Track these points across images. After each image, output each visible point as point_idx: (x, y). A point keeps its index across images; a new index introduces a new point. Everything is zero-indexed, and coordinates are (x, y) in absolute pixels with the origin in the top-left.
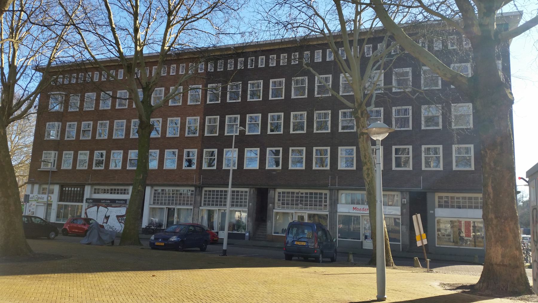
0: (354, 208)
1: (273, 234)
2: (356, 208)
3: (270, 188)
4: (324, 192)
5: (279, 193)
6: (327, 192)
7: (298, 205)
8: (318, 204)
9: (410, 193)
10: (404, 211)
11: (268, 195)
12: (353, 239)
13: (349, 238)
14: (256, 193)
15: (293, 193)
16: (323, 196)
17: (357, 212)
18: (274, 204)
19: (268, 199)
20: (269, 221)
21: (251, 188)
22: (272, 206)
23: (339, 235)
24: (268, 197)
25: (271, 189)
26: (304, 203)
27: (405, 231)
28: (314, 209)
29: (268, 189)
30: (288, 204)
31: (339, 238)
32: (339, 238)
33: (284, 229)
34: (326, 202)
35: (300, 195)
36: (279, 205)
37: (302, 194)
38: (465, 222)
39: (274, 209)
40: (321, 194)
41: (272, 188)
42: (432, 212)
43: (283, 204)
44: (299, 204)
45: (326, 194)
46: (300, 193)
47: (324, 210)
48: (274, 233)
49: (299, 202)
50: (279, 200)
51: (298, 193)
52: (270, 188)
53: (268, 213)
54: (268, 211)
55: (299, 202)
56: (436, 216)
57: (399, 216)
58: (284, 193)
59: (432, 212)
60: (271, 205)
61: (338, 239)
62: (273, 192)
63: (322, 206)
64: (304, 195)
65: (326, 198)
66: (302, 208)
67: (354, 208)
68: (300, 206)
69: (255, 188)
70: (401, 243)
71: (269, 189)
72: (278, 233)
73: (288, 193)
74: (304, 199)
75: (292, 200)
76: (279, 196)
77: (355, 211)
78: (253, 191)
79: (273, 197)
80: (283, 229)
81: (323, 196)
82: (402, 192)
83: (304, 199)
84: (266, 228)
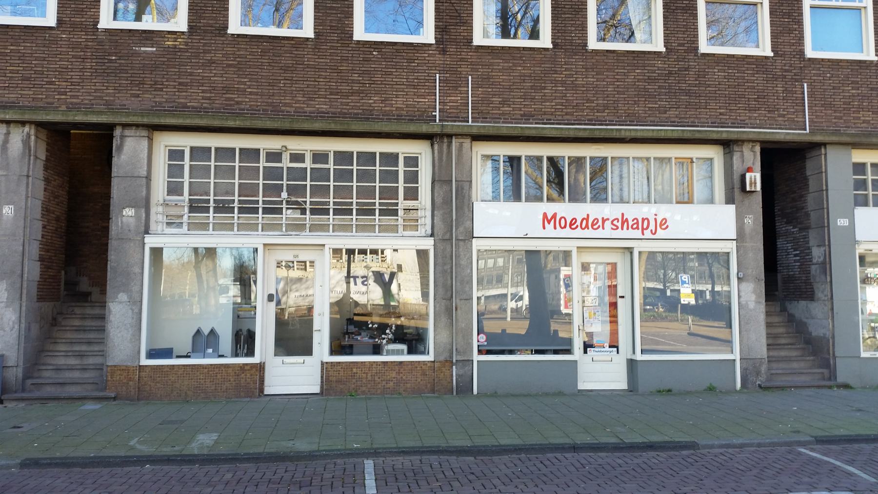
0: (545, 215)
1: (145, 362)
2: (554, 216)
3: (125, 126)
4: (403, 148)
5: (175, 154)
6: (421, 150)
7: (279, 211)
8: (354, 207)
9: (762, 142)
10: (749, 221)
11: (115, 160)
12: (538, 352)
13: (521, 352)
14: (42, 155)
15: (251, 154)
16: (401, 168)
17: (560, 233)
18: (147, 205)
19: (115, 182)
20: (123, 297)
21: (8, 122)
22: (137, 217)
23: (483, 338)
24: (114, 169)
25: (127, 132)
26: (355, 201)
27: (752, 305)
28: (241, 227)
29: (111, 127)
30: (223, 207)
31: (480, 352)
32: (480, 352)
33: (206, 331)
34: (412, 194)
35: (286, 163)
36: (173, 211)
37: (297, 157)
38: (209, 230)
39: (147, 232)
40: (391, 159)
41: (137, 126)
42: (843, 222)
43: (196, 207)
44: (284, 206)
45: (412, 161)
46: (286, 157)
47: (406, 233)
48: (151, 354)
49: (284, 195)
50: (174, 189)
51: (274, 156)
52: (125, 126)
53: (112, 256)
54: (113, 244)
55: (284, 195)
56: (858, 238)
57: (729, 244)
58: (198, 153)
59: (843, 222)
60: (129, 212)
61: (476, 357)
62: (145, 143)
63: (395, 213)
64: (308, 164)
65: (413, 177)
66: (299, 227)
67: (545, 215)
68: (289, 215)
69: (39, 125)
70: (736, 356)
71: (118, 132)
72: (167, 353)
73: (226, 153)
74: (308, 183)
75: (247, 190)
76: (175, 171)
77: (550, 230)
78: (26, 142)
79: (144, 173)
80: (198, 332)
81: (401, 168)
82: (727, 145)
83: (308, 183)
84: (102, 330)
